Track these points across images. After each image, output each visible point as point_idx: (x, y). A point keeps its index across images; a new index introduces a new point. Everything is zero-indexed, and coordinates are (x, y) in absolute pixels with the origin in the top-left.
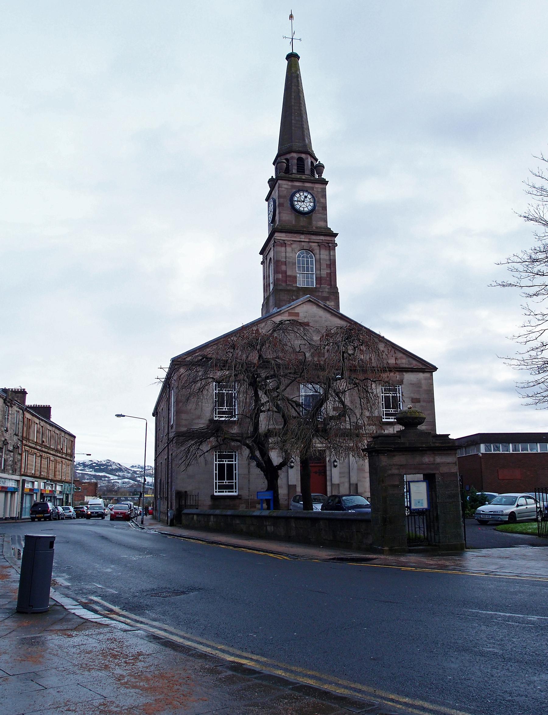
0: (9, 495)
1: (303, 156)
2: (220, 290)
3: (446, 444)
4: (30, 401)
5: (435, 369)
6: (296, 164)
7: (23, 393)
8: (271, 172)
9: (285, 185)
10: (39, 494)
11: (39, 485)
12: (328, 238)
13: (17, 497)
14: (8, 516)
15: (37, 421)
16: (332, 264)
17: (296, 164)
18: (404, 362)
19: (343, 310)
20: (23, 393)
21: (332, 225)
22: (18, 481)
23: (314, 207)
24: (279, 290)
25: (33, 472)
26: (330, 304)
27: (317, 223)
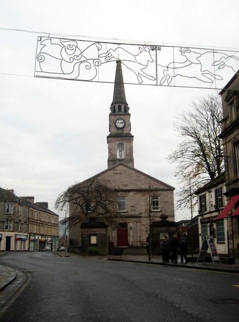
0: (23, 242)
1: (121, 104)
2: (92, 162)
3: (174, 224)
4: (36, 201)
5: (174, 189)
6: (119, 107)
7: (33, 198)
8: (110, 112)
9: (113, 117)
10: (38, 242)
11: (38, 237)
12: (130, 137)
13: (27, 242)
14: (22, 249)
15: (36, 211)
16: (131, 149)
17: (119, 107)
18: (161, 187)
19: (137, 166)
20: (33, 198)
21: (132, 133)
22: (27, 236)
23: (125, 126)
24: (113, 161)
25: (35, 232)
26: (130, 165)
27: (125, 131)
